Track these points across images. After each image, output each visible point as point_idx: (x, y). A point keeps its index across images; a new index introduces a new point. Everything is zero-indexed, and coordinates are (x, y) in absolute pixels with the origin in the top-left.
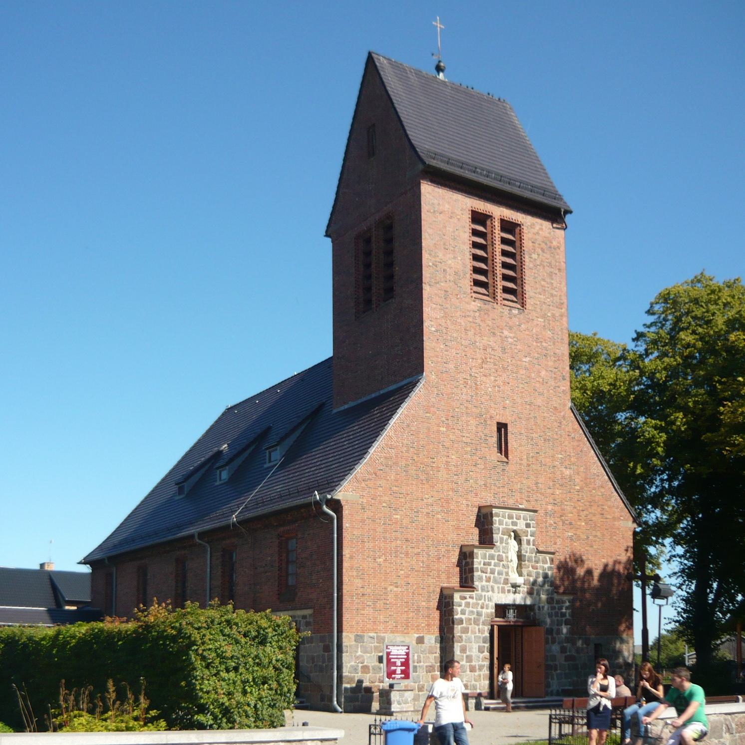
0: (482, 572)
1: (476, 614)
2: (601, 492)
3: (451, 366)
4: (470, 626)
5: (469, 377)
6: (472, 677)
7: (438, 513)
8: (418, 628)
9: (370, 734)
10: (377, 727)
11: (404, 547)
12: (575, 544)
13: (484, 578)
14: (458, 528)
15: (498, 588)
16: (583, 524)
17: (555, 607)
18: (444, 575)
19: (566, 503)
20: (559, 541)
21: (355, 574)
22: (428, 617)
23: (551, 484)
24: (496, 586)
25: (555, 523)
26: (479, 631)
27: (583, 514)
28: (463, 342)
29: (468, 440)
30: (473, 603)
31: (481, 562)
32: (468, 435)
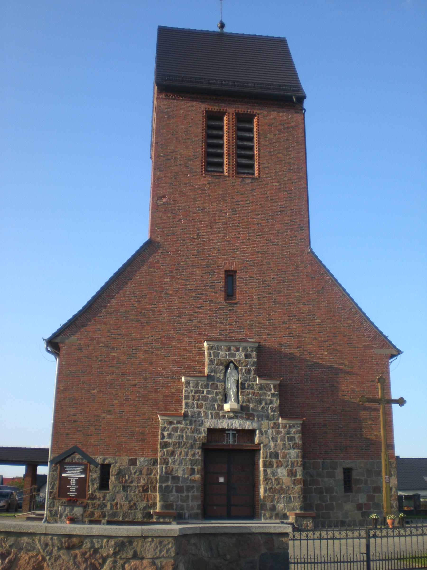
6: (178, 497)
10: (292, 538)
15: (211, 413)
16: (326, 353)
17: (281, 432)
19: (305, 335)
22: (143, 441)
29: (194, 287)
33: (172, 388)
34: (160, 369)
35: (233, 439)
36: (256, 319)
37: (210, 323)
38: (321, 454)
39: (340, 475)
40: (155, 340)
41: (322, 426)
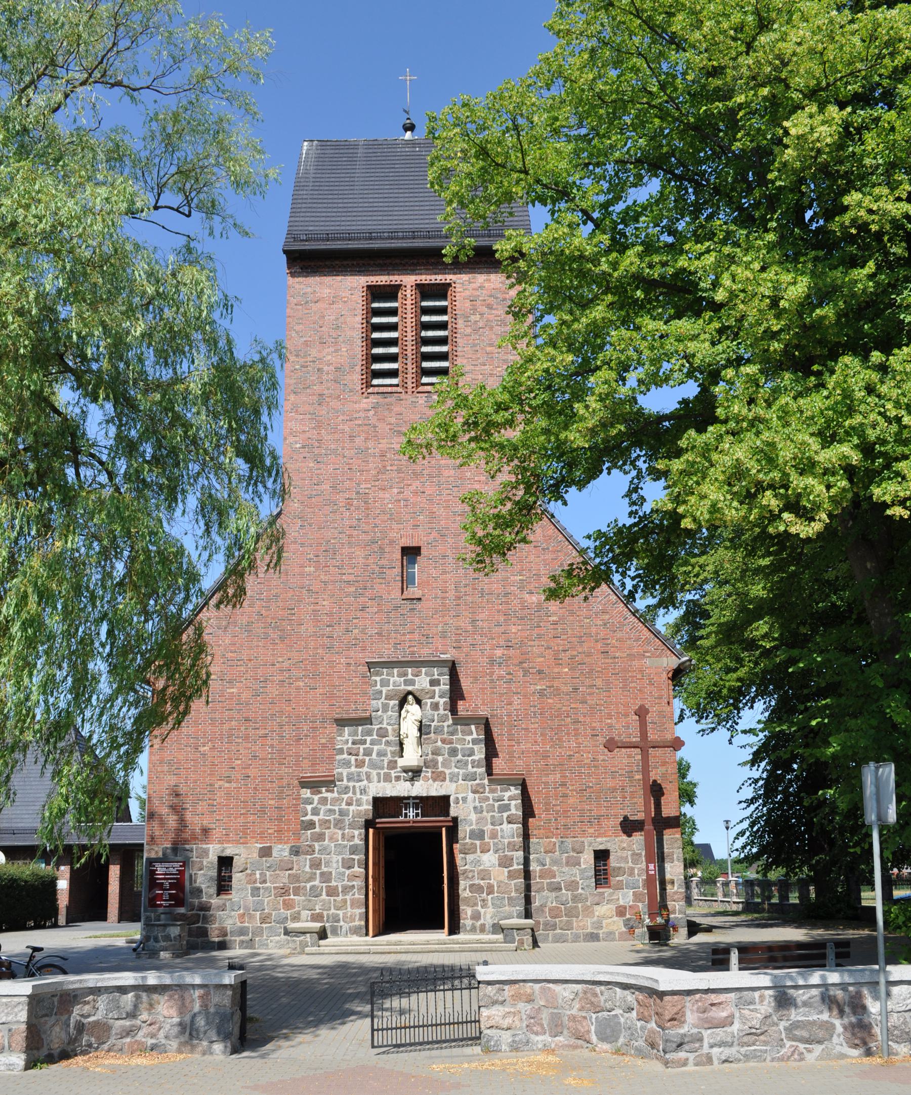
3: (326, 487)
5: (354, 496)
7: (298, 679)
8: (262, 836)
9: (373, 1030)
11: (243, 728)
12: (550, 701)
13: (353, 762)
14: (332, 696)
15: (378, 775)
18: (306, 761)
20: (516, 700)
21: (166, 768)
22: (279, 820)
23: (502, 619)
28: (347, 453)
29: (352, 578)
30: (332, 799)
32: (350, 571)
37: (379, 634)
39: (587, 860)
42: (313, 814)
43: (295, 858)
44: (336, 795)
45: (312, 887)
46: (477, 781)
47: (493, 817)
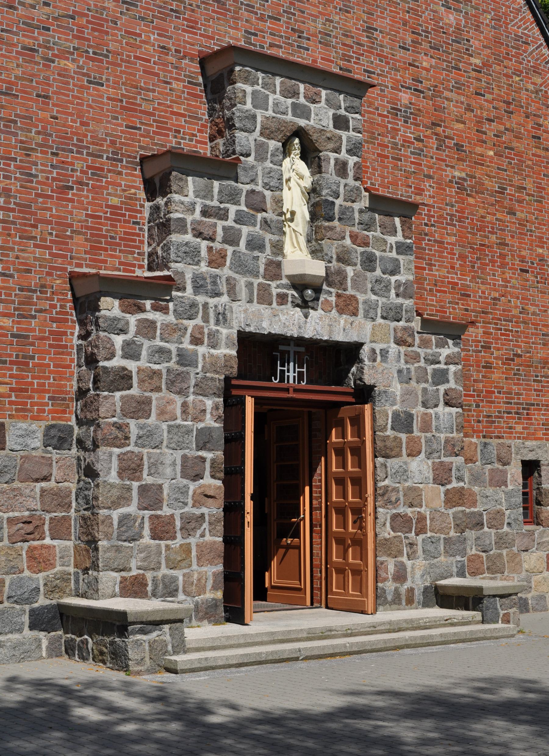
0: (199, 234)
1: (174, 359)
2: (535, 84)
4: (154, 396)
7: (64, 54)
12: (471, 200)
13: (204, 253)
15: (250, 285)
16: (491, 153)
18: (78, 239)
19: (446, 94)
24: (242, 281)
25: (418, 139)
26: (185, 412)
27: (491, 129)
30: (166, 326)
31: (194, 204)
33: (110, 191)
34: (72, 121)
35: (297, 370)
36: (337, 18)
38: (479, 422)
40: (55, 19)
41: (482, 347)
42: (126, 356)
43: (55, 454)
44: (171, 318)
45: (124, 519)
46: (402, 323)
47: (425, 390)
